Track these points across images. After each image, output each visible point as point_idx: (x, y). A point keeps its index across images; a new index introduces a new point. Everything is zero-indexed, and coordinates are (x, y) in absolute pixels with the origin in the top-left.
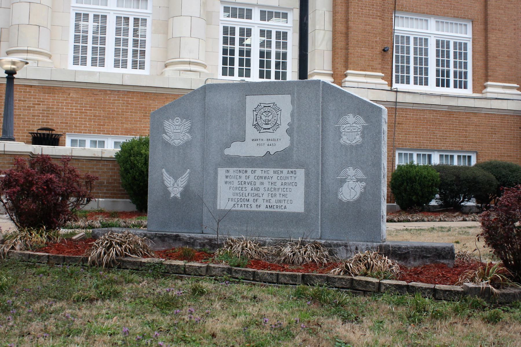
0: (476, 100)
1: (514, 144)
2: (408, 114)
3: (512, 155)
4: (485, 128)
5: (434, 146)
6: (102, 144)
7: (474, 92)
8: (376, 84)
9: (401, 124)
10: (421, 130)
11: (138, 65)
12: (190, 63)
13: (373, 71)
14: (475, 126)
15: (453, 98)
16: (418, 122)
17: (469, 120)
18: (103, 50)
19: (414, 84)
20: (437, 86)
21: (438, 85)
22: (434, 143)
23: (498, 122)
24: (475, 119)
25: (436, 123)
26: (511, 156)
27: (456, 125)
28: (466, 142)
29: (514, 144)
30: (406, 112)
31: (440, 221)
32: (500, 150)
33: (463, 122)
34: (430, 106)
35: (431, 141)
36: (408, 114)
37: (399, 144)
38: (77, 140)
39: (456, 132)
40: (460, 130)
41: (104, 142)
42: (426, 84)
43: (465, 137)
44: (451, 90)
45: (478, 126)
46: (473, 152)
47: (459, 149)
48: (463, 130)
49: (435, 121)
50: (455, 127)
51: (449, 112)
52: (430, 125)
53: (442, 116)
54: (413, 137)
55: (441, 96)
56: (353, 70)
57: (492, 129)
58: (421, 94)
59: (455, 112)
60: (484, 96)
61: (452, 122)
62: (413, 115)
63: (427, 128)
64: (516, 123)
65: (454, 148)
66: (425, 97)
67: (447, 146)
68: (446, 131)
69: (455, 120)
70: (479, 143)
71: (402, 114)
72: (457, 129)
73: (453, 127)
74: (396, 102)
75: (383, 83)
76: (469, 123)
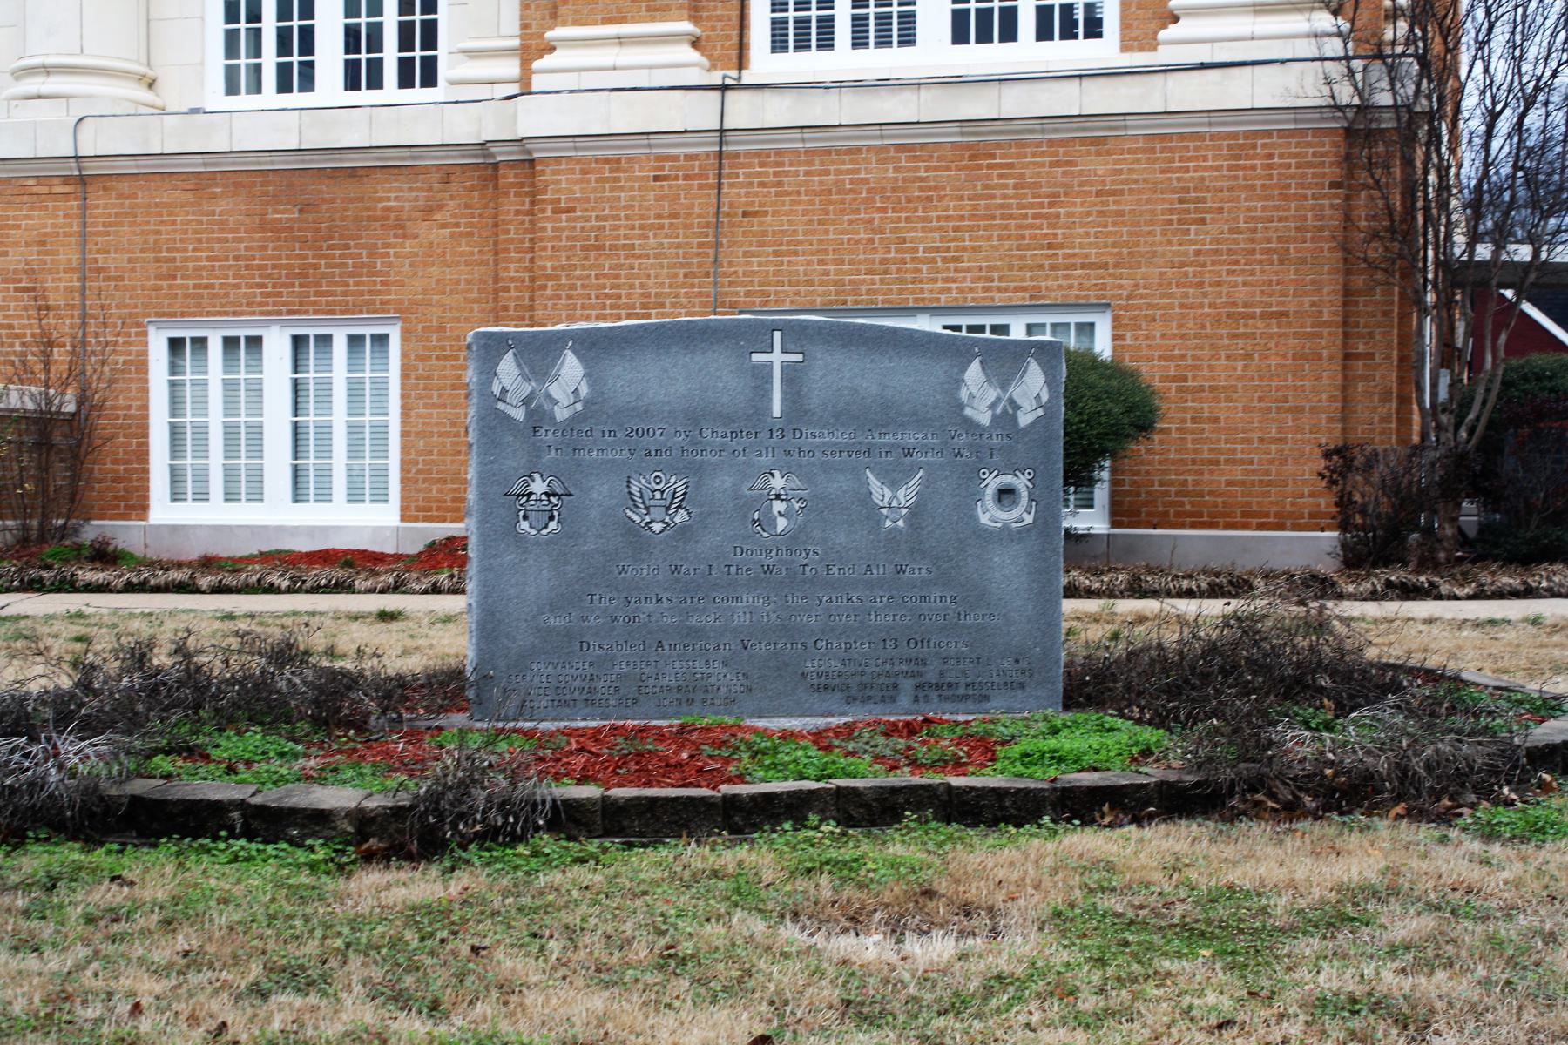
0: (1086, 82)
1: (1303, 261)
2: (787, 174)
3: (1292, 308)
4: (1148, 201)
5: (900, 291)
6: (1030, 329)
7: (1125, 47)
8: (651, 67)
9: (755, 214)
10: (843, 232)
11: (420, 72)
12: (47, 70)
13: (653, 20)
14: (1098, 194)
15: (1128, 78)
16: (830, 202)
17: (1065, 174)
18: (307, 35)
19: (855, 45)
20: (774, 50)
21: (960, 36)
22: (902, 281)
23: (1218, 168)
24: (1098, 167)
25: (909, 200)
26: (1284, 314)
27: (1004, 197)
28: (1053, 268)
29: (1303, 261)
30: (778, 164)
31: (435, 589)
32: (1224, 290)
33: (1037, 185)
34: (876, 131)
35: (886, 272)
36: (787, 174)
37: (748, 294)
38: (1068, 324)
39: (1006, 227)
40: (1025, 217)
41: (1092, 325)
42: (908, 39)
43: (1050, 246)
44: (843, 60)
45: (1113, 193)
46: (1103, 307)
47: (1018, 298)
48: (1035, 216)
49: (904, 190)
50: (1002, 206)
51: (969, 146)
52: (883, 210)
53: (936, 169)
54: (809, 263)
55: (883, 84)
56: (576, 23)
57: (1181, 201)
58: (840, 85)
59: (998, 145)
60: (1163, 56)
61: (986, 187)
62: (807, 173)
63: (871, 221)
64: (1311, 165)
65: (998, 296)
66: (848, 97)
67: (960, 290)
68: (956, 229)
69: (1000, 176)
70: (1116, 265)
71: (759, 174)
72: (1011, 217)
73: (988, 207)
74: (722, 131)
75: (688, 63)
76: (1065, 185)
